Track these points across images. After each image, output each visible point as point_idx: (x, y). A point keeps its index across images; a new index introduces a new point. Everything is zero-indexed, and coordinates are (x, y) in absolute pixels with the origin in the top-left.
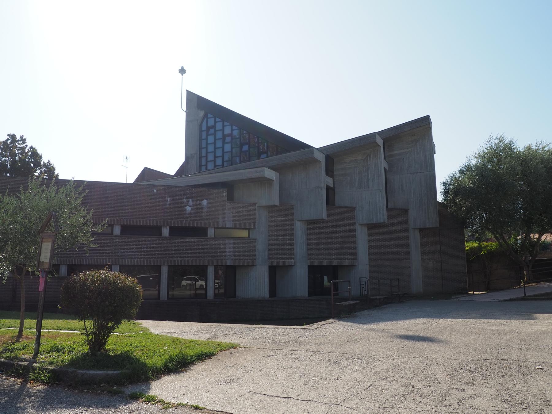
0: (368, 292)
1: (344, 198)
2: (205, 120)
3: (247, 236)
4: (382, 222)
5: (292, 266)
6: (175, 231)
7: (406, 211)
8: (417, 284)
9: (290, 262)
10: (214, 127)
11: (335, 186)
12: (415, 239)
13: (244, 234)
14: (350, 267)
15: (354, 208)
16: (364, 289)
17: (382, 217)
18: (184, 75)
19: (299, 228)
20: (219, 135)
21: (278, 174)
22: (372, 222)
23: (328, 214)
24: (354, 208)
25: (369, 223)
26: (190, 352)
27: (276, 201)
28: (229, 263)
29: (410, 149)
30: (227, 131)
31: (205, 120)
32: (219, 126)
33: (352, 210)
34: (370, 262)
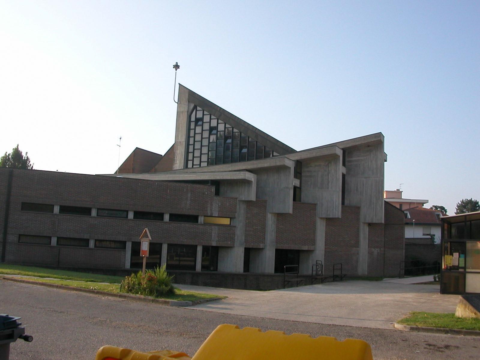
0: (322, 272)
1: (307, 196)
2: (195, 111)
3: (229, 223)
4: (337, 217)
5: (262, 249)
6: (174, 217)
7: (359, 208)
8: (363, 268)
9: (261, 246)
10: (202, 119)
11: (302, 185)
12: (364, 232)
13: (226, 221)
14: (309, 252)
15: (316, 205)
16: (319, 269)
17: (337, 213)
18: (178, 70)
19: (270, 220)
20: (206, 127)
21: (256, 176)
22: (329, 217)
23: (294, 208)
24: (316, 205)
25: (327, 217)
26: (203, 298)
27: (253, 198)
28: (214, 244)
29: (365, 158)
30: (214, 123)
31: (195, 111)
32: (207, 119)
33: (313, 206)
34: (325, 248)
